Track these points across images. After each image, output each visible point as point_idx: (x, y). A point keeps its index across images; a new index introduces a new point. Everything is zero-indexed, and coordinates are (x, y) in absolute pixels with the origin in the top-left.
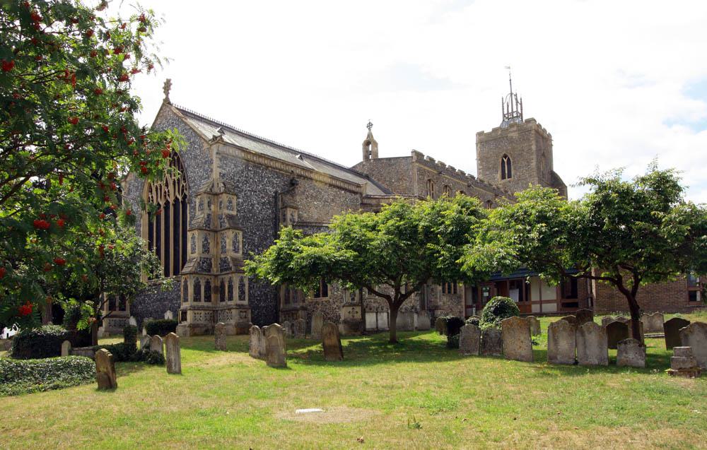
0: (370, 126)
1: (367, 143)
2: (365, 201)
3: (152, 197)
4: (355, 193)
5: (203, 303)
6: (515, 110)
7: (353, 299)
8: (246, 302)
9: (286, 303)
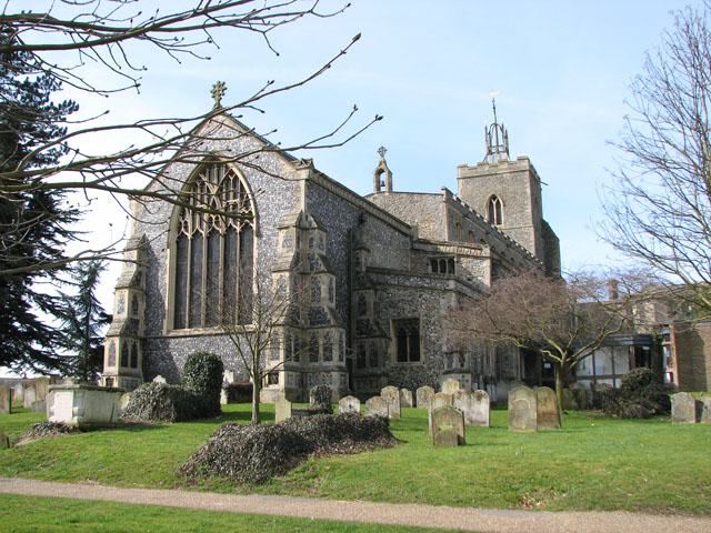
0: (382, 151)
1: (380, 172)
2: (417, 246)
3: (186, 223)
4: (406, 235)
5: (293, 363)
6: (501, 143)
7: (462, 365)
8: (343, 364)
9: (359, 367)
